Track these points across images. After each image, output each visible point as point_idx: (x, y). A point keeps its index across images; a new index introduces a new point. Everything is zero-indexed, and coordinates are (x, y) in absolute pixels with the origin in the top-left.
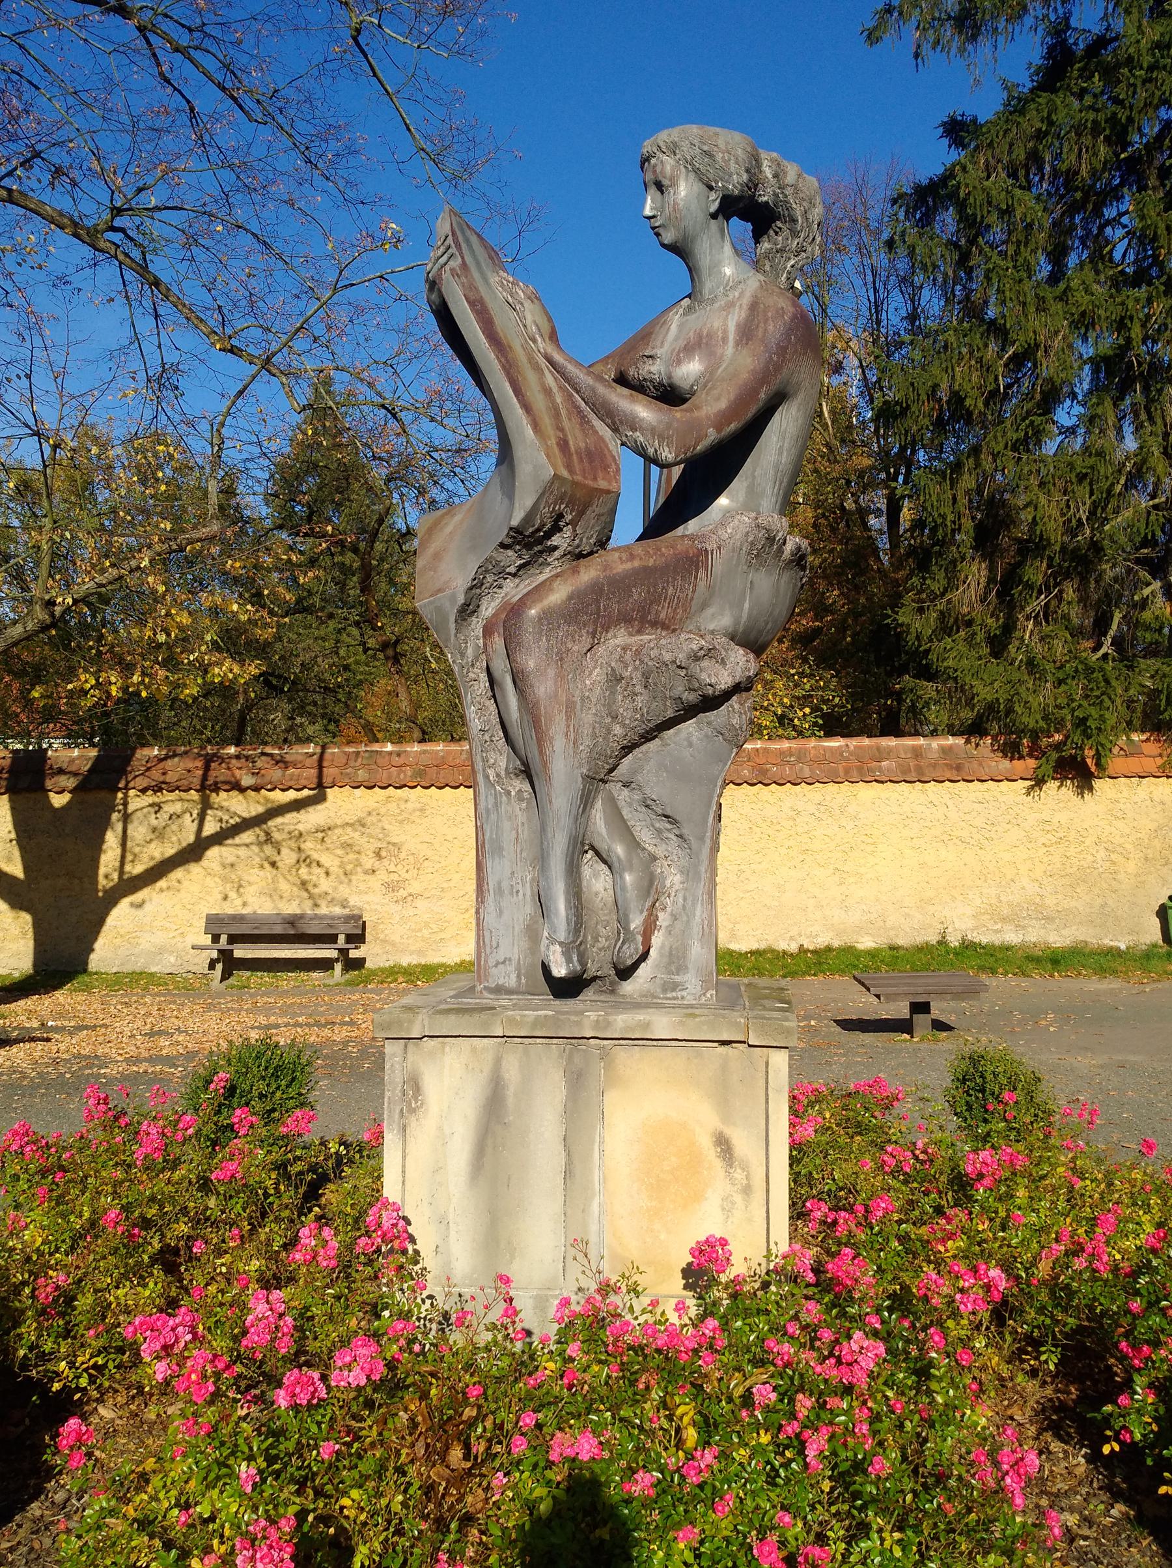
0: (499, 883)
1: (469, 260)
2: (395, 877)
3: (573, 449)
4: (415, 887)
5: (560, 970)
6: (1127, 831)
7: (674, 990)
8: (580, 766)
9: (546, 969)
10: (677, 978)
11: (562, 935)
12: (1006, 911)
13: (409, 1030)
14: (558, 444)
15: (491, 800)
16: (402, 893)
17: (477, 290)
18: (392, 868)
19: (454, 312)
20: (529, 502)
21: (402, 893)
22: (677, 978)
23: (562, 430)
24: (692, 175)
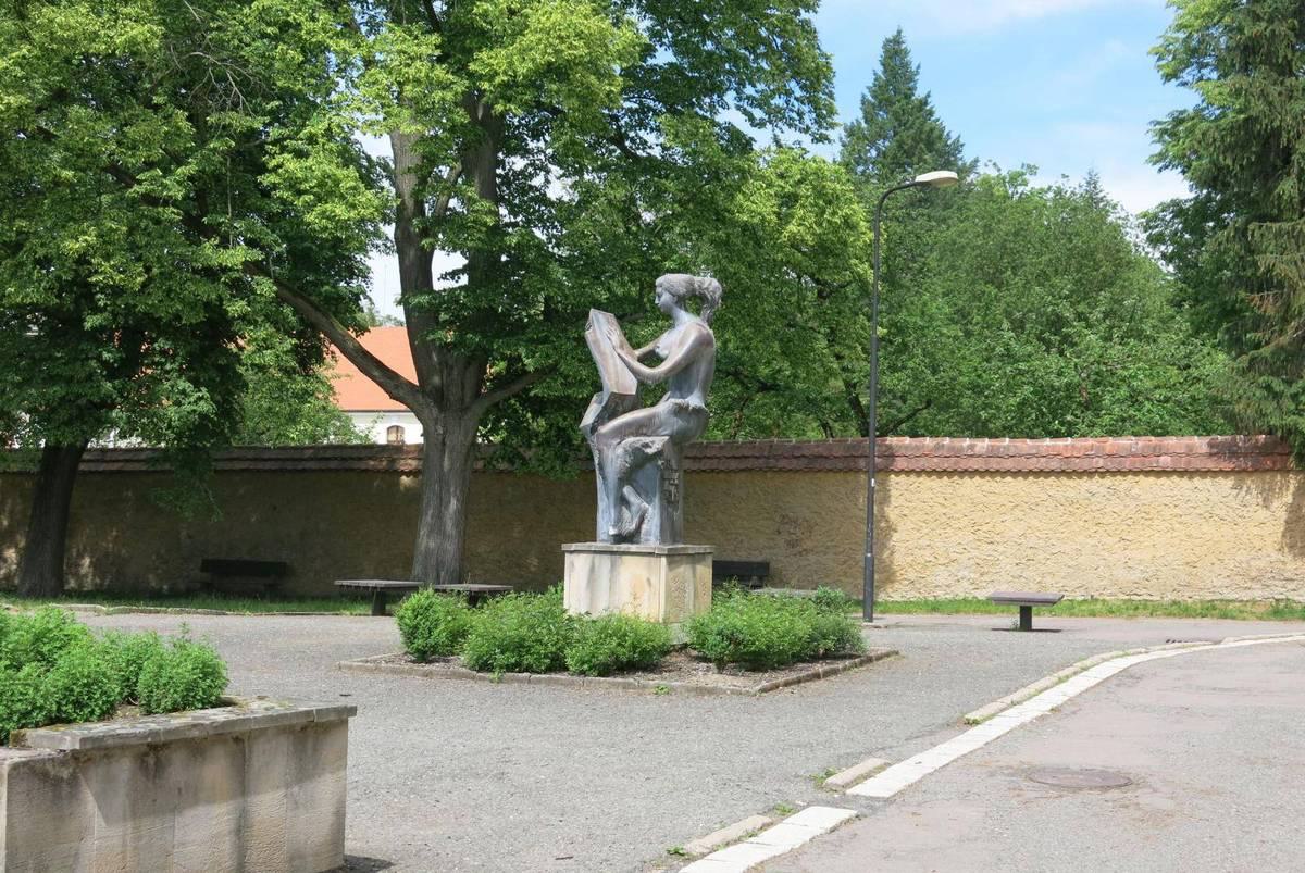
4: (808, 544)
12: (1253, 574)
21: (799, 549)
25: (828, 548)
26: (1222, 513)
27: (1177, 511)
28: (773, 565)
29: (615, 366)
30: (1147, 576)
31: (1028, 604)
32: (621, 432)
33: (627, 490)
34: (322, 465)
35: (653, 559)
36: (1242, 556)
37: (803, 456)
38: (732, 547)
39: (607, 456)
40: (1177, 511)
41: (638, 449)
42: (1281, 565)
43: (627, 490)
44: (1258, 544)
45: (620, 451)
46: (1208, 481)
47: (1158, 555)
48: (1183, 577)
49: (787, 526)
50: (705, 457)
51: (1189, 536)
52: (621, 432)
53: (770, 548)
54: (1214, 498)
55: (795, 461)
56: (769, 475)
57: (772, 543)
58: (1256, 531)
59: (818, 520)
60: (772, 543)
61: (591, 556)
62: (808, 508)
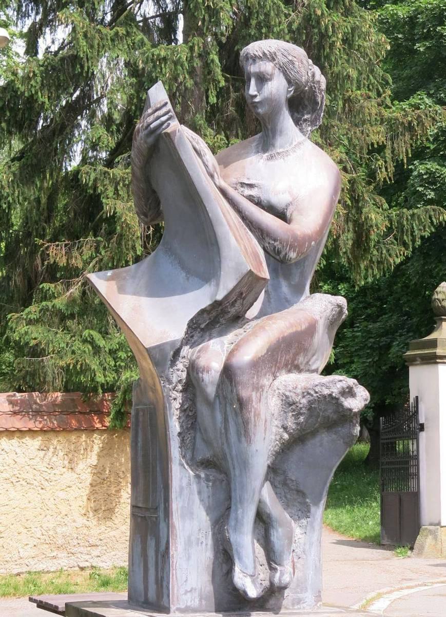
7: (298, 603)
10: (300, 596)
24: (282, 75)
26: (30, 477)
41: (332, 400)
42: (85, 531)
46: (15, 441)
54: (21, 460)
58: (62, 495)
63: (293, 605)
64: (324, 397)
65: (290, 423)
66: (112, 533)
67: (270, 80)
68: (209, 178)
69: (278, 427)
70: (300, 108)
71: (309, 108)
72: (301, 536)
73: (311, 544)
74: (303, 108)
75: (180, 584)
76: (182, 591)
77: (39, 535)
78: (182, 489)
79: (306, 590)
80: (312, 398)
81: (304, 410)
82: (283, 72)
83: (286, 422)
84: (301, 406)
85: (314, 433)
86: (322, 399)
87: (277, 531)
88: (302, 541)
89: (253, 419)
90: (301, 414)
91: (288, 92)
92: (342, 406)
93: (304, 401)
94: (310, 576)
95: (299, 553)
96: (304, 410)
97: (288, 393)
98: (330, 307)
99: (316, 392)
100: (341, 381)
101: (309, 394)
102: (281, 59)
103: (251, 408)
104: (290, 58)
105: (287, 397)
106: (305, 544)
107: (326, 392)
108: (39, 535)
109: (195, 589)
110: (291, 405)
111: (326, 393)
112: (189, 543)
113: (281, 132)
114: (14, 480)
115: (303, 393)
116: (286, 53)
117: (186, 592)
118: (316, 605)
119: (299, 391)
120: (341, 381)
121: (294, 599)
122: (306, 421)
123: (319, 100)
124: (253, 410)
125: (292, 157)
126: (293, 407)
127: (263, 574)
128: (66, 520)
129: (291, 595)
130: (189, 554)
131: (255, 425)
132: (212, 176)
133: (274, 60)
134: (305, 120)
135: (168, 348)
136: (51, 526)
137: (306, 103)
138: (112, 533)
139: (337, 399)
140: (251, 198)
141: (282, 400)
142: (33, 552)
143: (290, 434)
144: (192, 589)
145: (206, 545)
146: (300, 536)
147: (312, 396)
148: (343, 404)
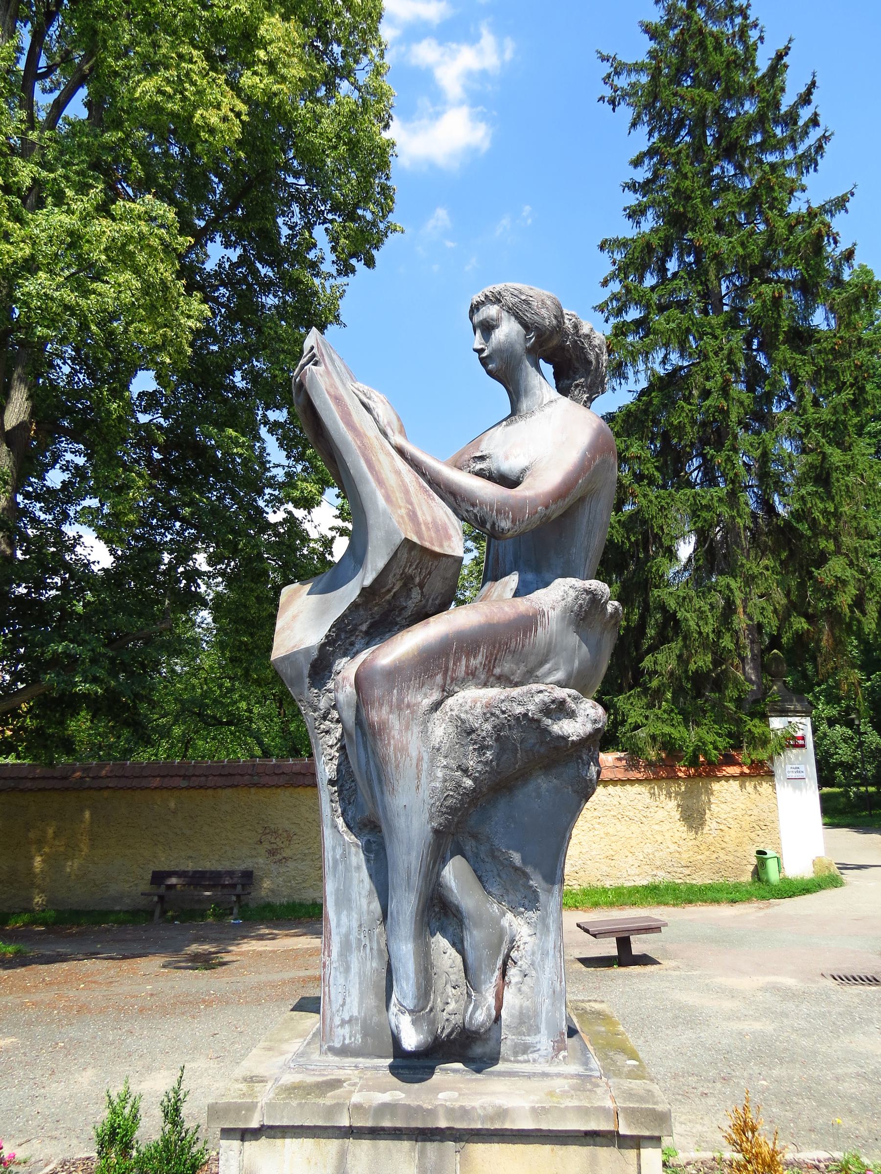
0: (347, 936)
1: (330, 367)
2: (275, 846)
3: (421, 520)
4: (287, 853)
5: (411, 1040)
6: (729, 810)
7: (525, 1052)
8: (431, 818)
9: (396, 1041)
10: (529, 1039)
11: (410, 1003)
12: (658, 863)
13: (247, 1119)
14: (408, 515)
15: (339, 851)
16: (279, 857)
17: (337, 388)
18: (273, 840)
19: (317, 403)
20: (381, 564)
21: (279, 857)
22: (529, 1039)
23: (411, 504)
24: (513, 319)
25: (305, 855)
26: (631, 814)
27: (596, 814)
28: (256, 873)
29: (398, 473)
30: (576, 869)
31: (625, 935)
32: (440, 666)
33: (454, 874)
34: (167, 782)
35: (606, 1154)
36: (649, 849)
37: (283, 773)
38: (217, 857)
39: (404, 750)
40: (596, 814)
41: (526, 722)
42: (677, 855)
43: (454, 874)
44: (660, 838)
45: (441, 730)
46: (618, 788)
47: (584, 851)
48: (605, 868)
49: (269, 837)
50: (194, 775)
51: (607, 834)
52: (440, 666)
53: (253, 857)
54: (623, 802)
55: (276, 778)
56: (253, 790)
57: (254, 853)
58: (657, 827)
59: (297, 830)
60: (254, 853)
61: (333, 1145)
62: (288, 819)
63: (516, 1054)
64: (517, 718)
65: (471, 763)
66: (699, 857)
67: (497, 326)
68: (382, 437)
69: (452, 769)
70: (571, 373)
71: (582, 370)
72: (528, 939)
73: (545, 954)
74: (575, 373)
75: (334, 1010)
76: (337, 1021)
77: (641, 858)
78: (335, 862)
79: (538, 1031)
80: (497, 721)
81: (489, 742)
82: (514, 315)
83: (464, 761)
84: (484, 733)
85: (523, 776)
86: (513, 722)
87: (471, 933)
88: (528, 947)
89: (392, 756)
90: (487, 748)
91: (527, 340)
92: (550, 733)
93: (488, 726)
94: (544, 1009)
95: (525, 967)
96: (489, 742)
97: (463, 716)
98: (572, 593)
99: (504, 712)
100: (541, 692)
101: (493, 714)
102: (509, 299)
103: (389, 740)
104: (523, 297)
105: (463, 722)
106: (533, 954)
107: (519, 710)
108: (641, 858)
109: (357, 1019)
110: (469, 734)
111: (518, 712)
112: (346, 947)
113: (526, 391)
114: (620, 816)
115: (485, 714)
116: (516, 292)
117: (343, 1023)
118: (557, 1056)
119: (479, 710)
120: (541, 692)
121: (516, 1045)
122: (498, 757)
123: (592, 358)
124: (392, 742)
125: (538, 415)
126: (474, 736)
127: (457, 1002)
128: (662, 846)
129: (510, 1037)
130: (347, 962)
131: (397, 766)
132: (385, 434)
133: (500, 301)
134: (577, 386)
135: (302, 658)
136: (650, 851)
137: (577, 365)
138: (699, 857)
139: (538, 721)
140: (480, 474)
141: (457, 727)
142: (637, 871)
143: (475, 780)
144: (351, 1017)
145: (371, 949)
146: (528, 939)
147: (498, 717)
148: (550, 728)
